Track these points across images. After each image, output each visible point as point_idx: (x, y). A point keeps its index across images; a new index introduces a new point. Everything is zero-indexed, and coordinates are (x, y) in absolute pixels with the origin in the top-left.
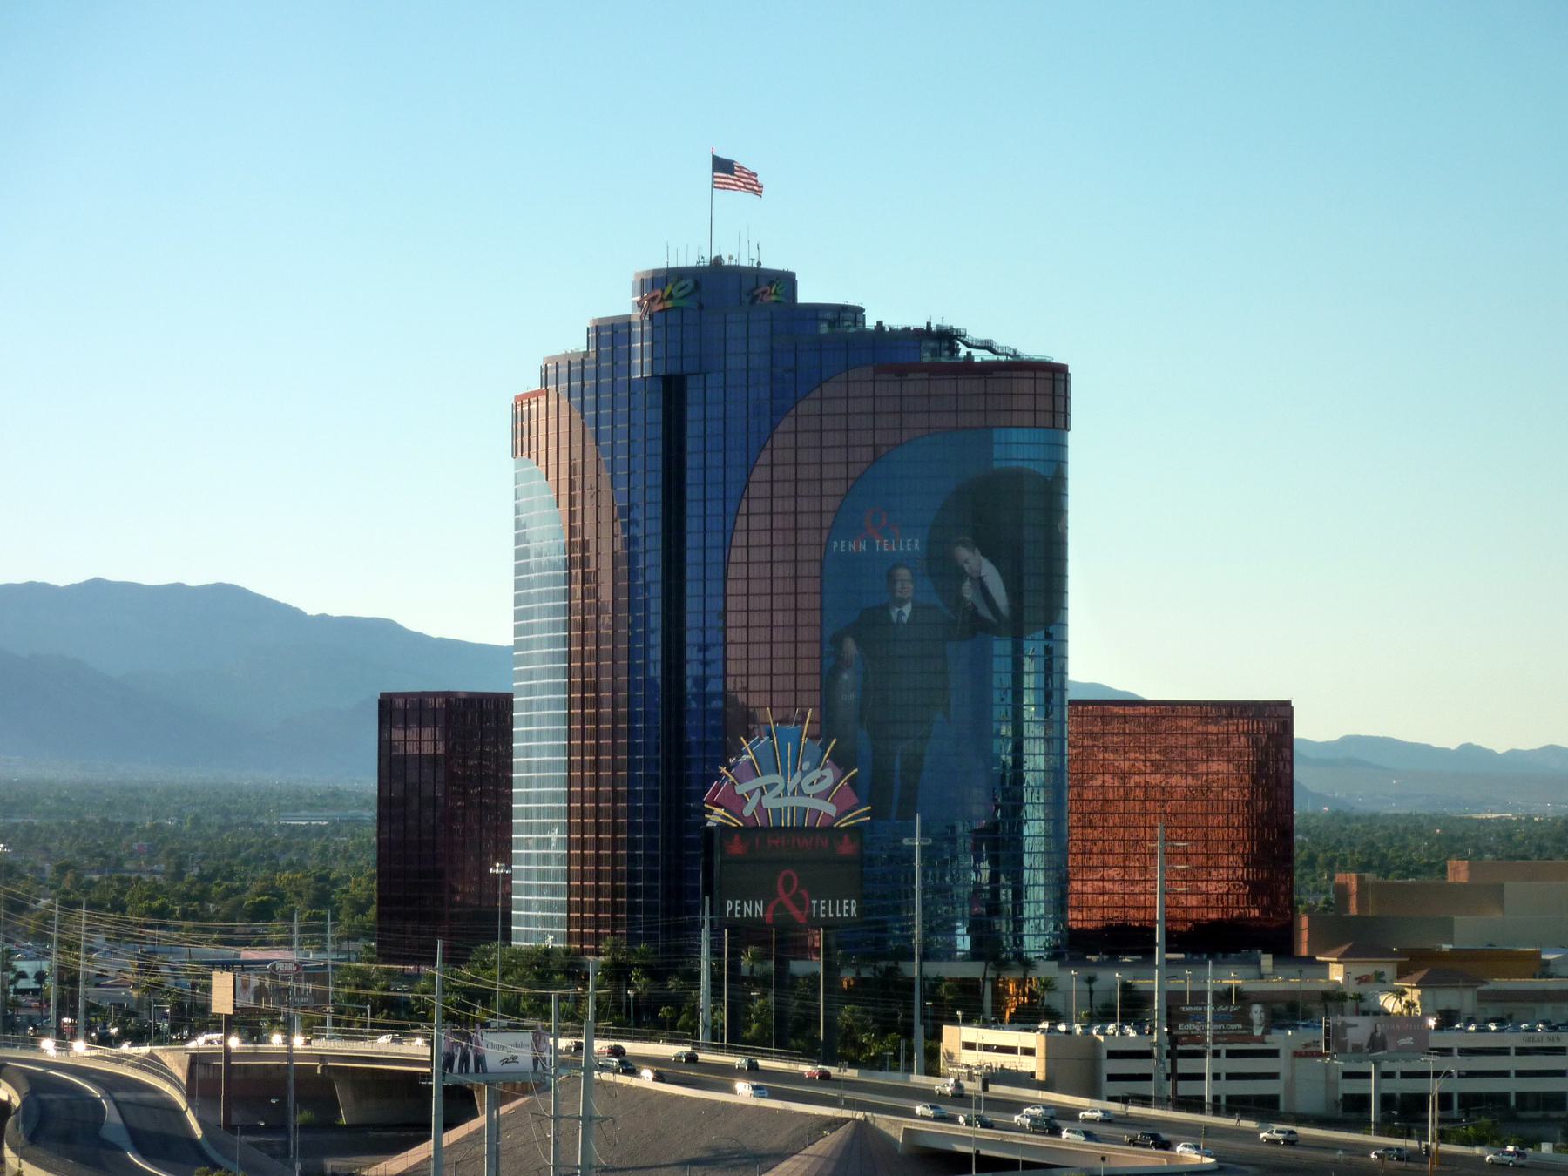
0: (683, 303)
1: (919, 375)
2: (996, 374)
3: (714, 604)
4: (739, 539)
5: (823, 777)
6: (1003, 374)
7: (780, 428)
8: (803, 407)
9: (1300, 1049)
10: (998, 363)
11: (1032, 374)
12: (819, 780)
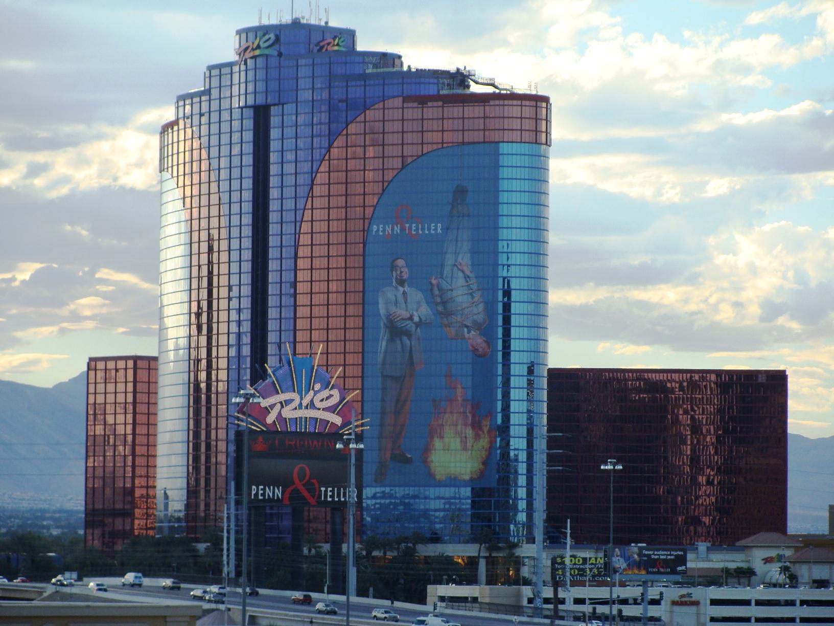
0: (267, 52)
1: (435, 104)
2: (492, 103)
3: (288, 277)
4: (306, 227)
5: (331, 396)
6: (497, 102)
7: (335, 144)
8: (352, 128)
9: (677, 599)
10: (499, 94)
11: (519, 103)
12: (327, 398)
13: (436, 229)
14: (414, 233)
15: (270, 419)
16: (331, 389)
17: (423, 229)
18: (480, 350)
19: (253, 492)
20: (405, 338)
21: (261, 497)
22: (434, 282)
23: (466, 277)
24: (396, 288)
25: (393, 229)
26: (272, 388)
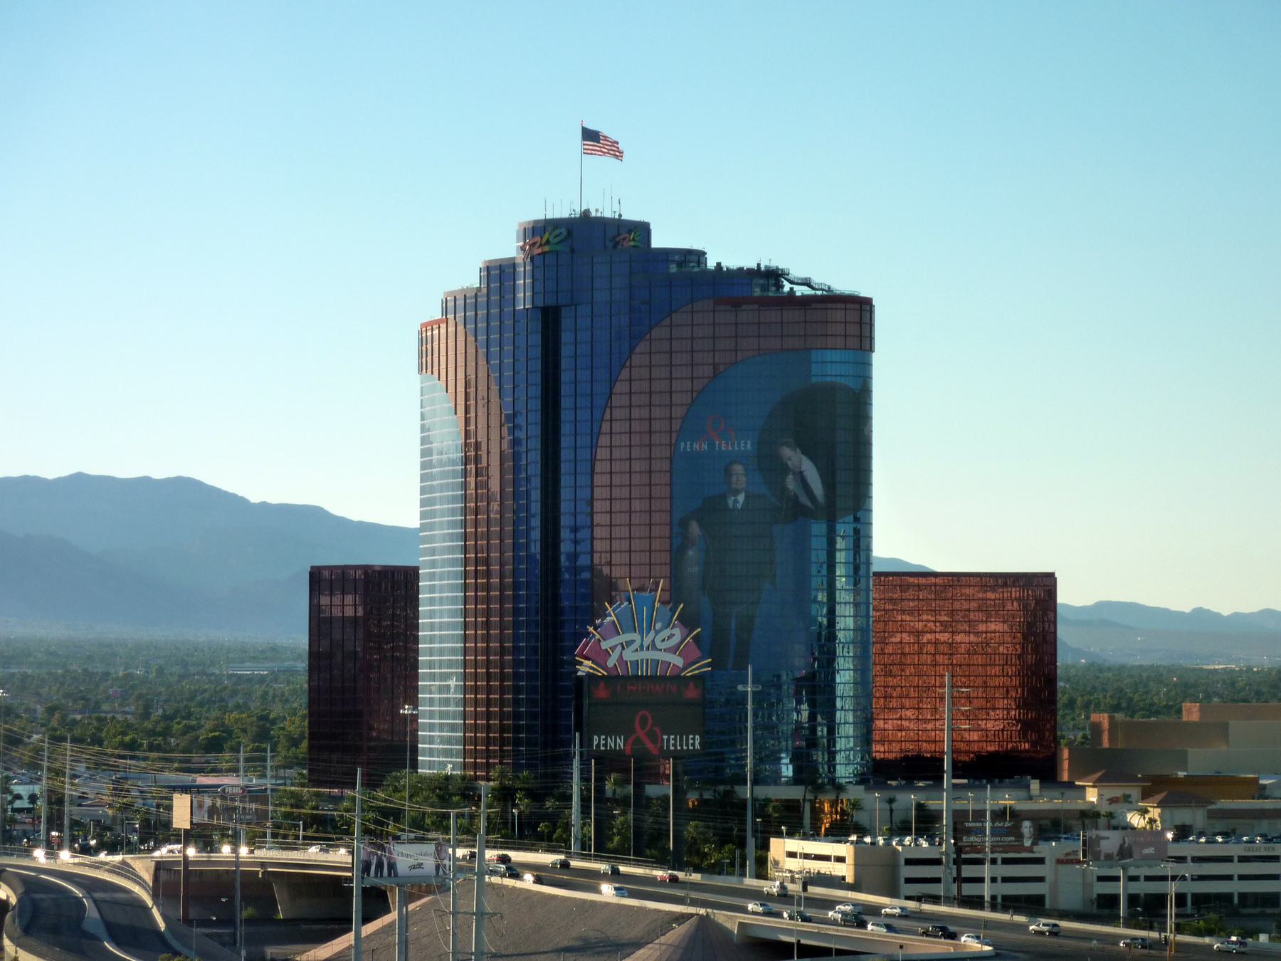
0: (558, 248)
1: (751, 307)
2: (813, 306)
3: (584, 494)
4: (604, 440)
5: (673, 635)
6: (819, 306)
7: (637, 350)
8: (656, 333)
9: (1062, 857)
10: (815, 296)
11: (843, 306)
12: (669, 638)
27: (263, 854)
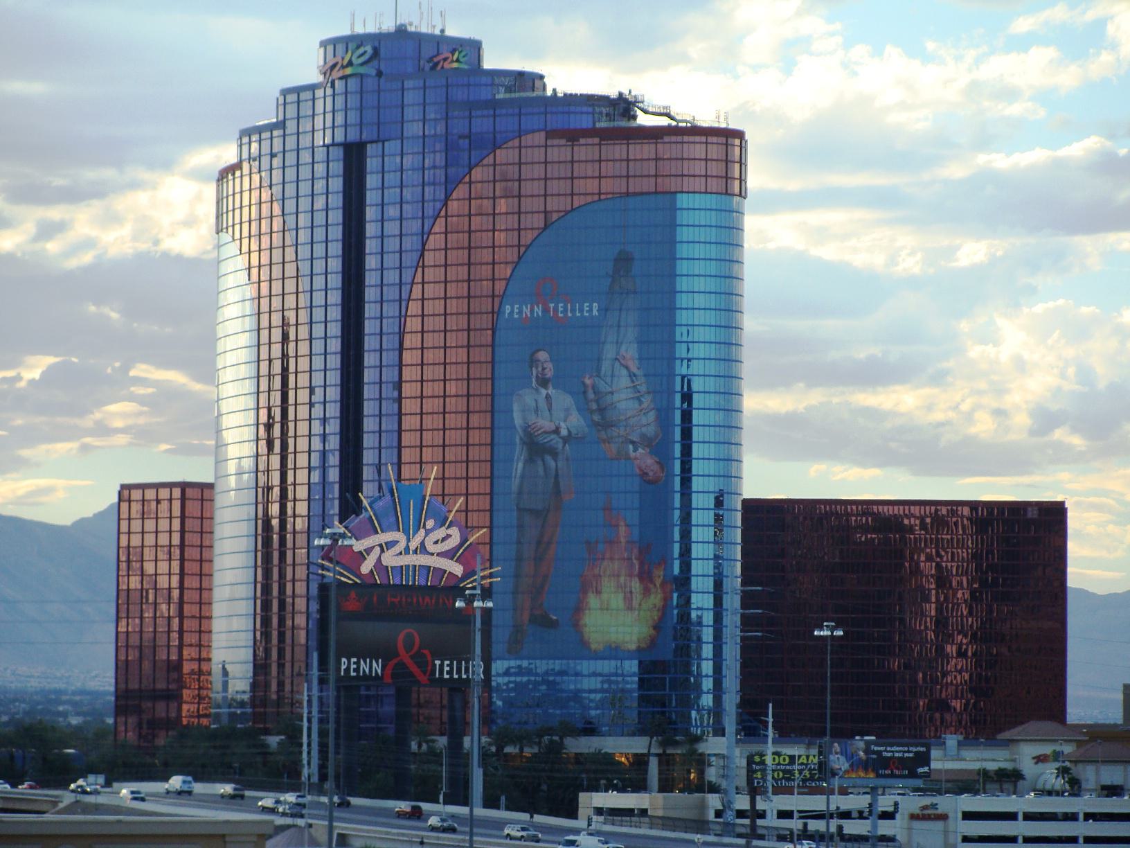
0: (362, 70)
1: (590, 141)
2: (666, 139)
3: (390, 375)
4: (414, 308)
5: (449, 536)
6: (674, 139)
7: (454, 195)
8: (477, 174)
9: (917, 811)
10: (677, 127)
11: (703, 139)
12: (444, 539)
13: (591, 310)
14: (560, 315)
15: (366, 568)
16: (449, 527)
17: (573, 310)
18: (651, 474)
19: (343, 667)
20: (548, 458)
21: (353, 674)
22: (588, 381)
23: (632, 376)
24: (537, 390)
25: (532, 310)
26: (369, 526)
27: (476, 700)
